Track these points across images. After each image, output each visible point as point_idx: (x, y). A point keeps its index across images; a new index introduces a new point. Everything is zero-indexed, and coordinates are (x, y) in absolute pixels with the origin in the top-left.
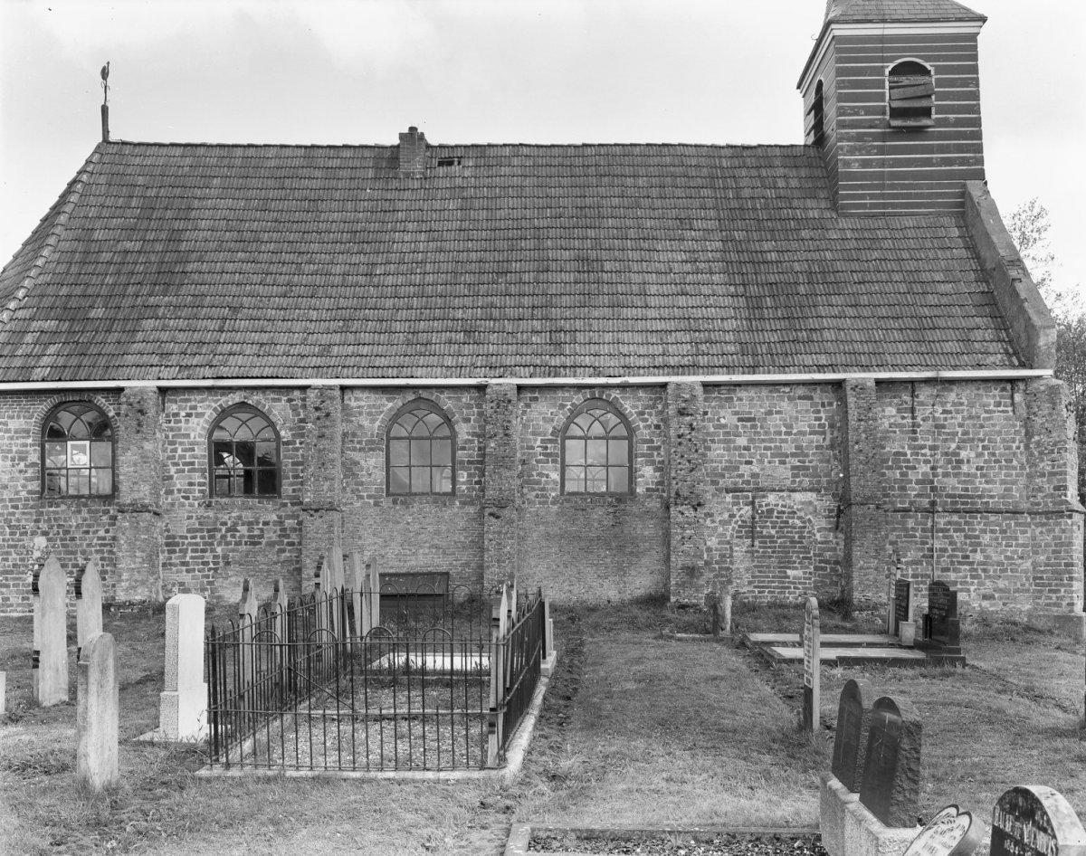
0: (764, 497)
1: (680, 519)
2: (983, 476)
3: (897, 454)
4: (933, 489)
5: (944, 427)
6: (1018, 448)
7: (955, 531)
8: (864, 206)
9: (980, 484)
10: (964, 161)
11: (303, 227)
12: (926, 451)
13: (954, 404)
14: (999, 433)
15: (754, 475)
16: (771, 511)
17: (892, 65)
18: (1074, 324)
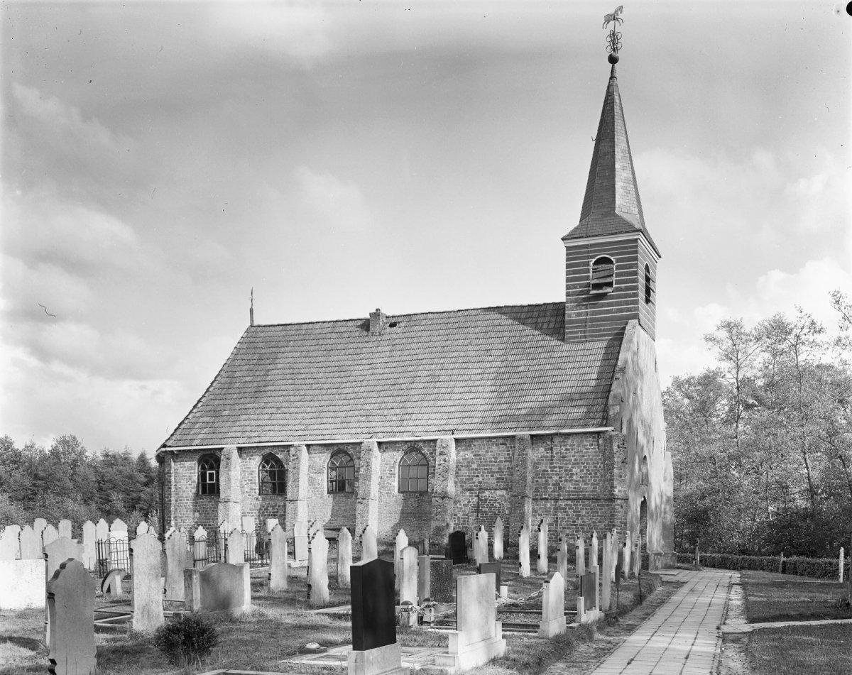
0: (484, 492)
1: (436, 504)
2: (583, 481)
3: (544, 471)
4: (560, 488)
5: (565, 457)
6: (600, 467)
7: (569, 509)
8: (577, 337)
9: (582, 485)
10: (628, 310)
11: (320, 365)
12: (558, 469)
13: (571, 445)
14: (592, 459)
15: (480, 483)
16: (486, 500)
17: (594, 260)
18: (173, 463)
